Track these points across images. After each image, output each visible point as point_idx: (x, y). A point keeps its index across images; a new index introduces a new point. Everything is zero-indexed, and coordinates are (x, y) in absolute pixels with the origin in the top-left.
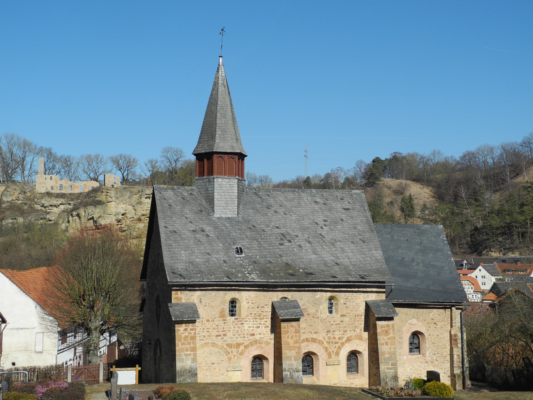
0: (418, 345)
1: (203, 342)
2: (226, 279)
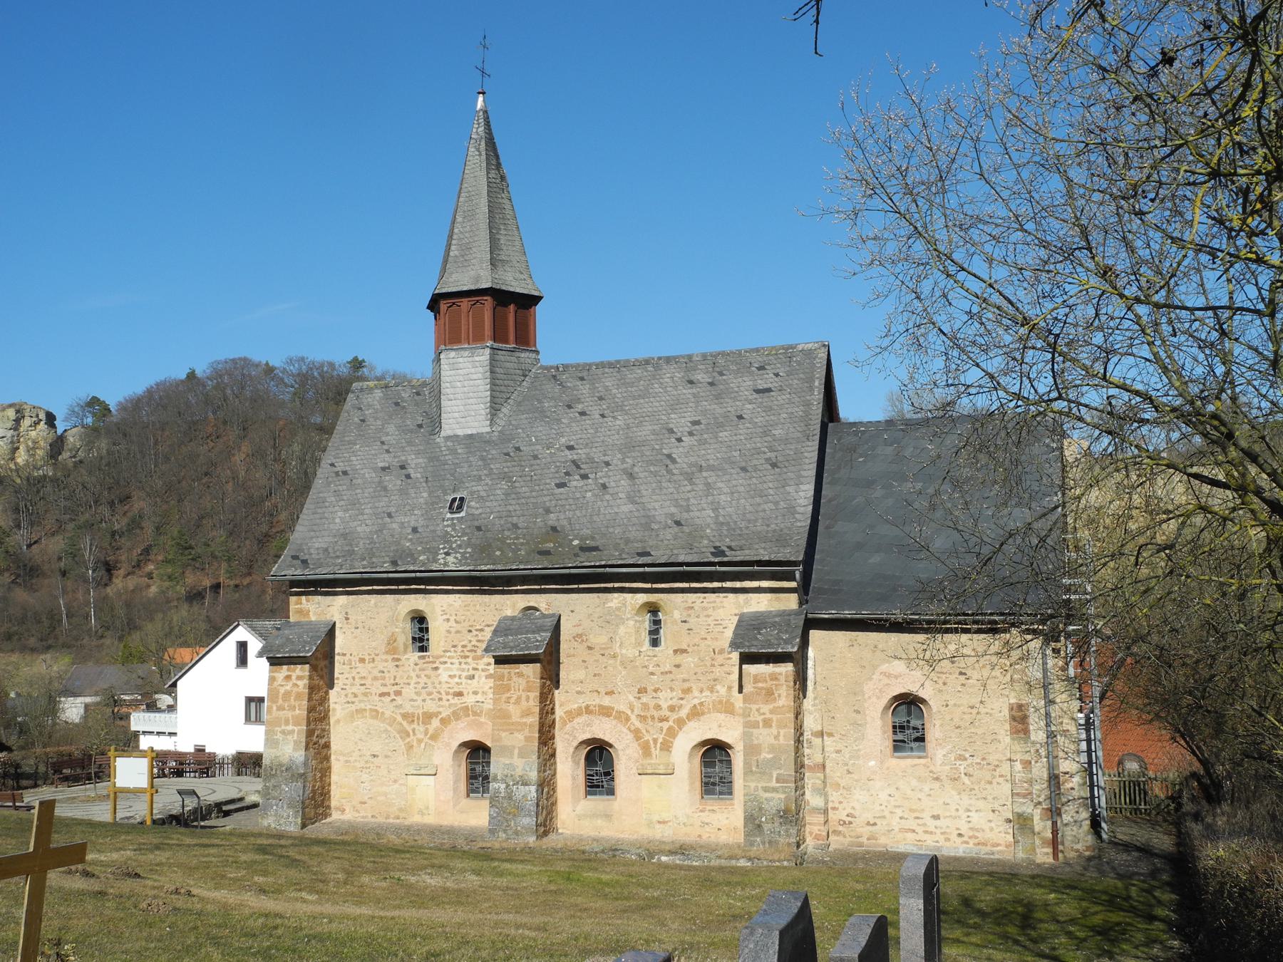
1: (353, 707)
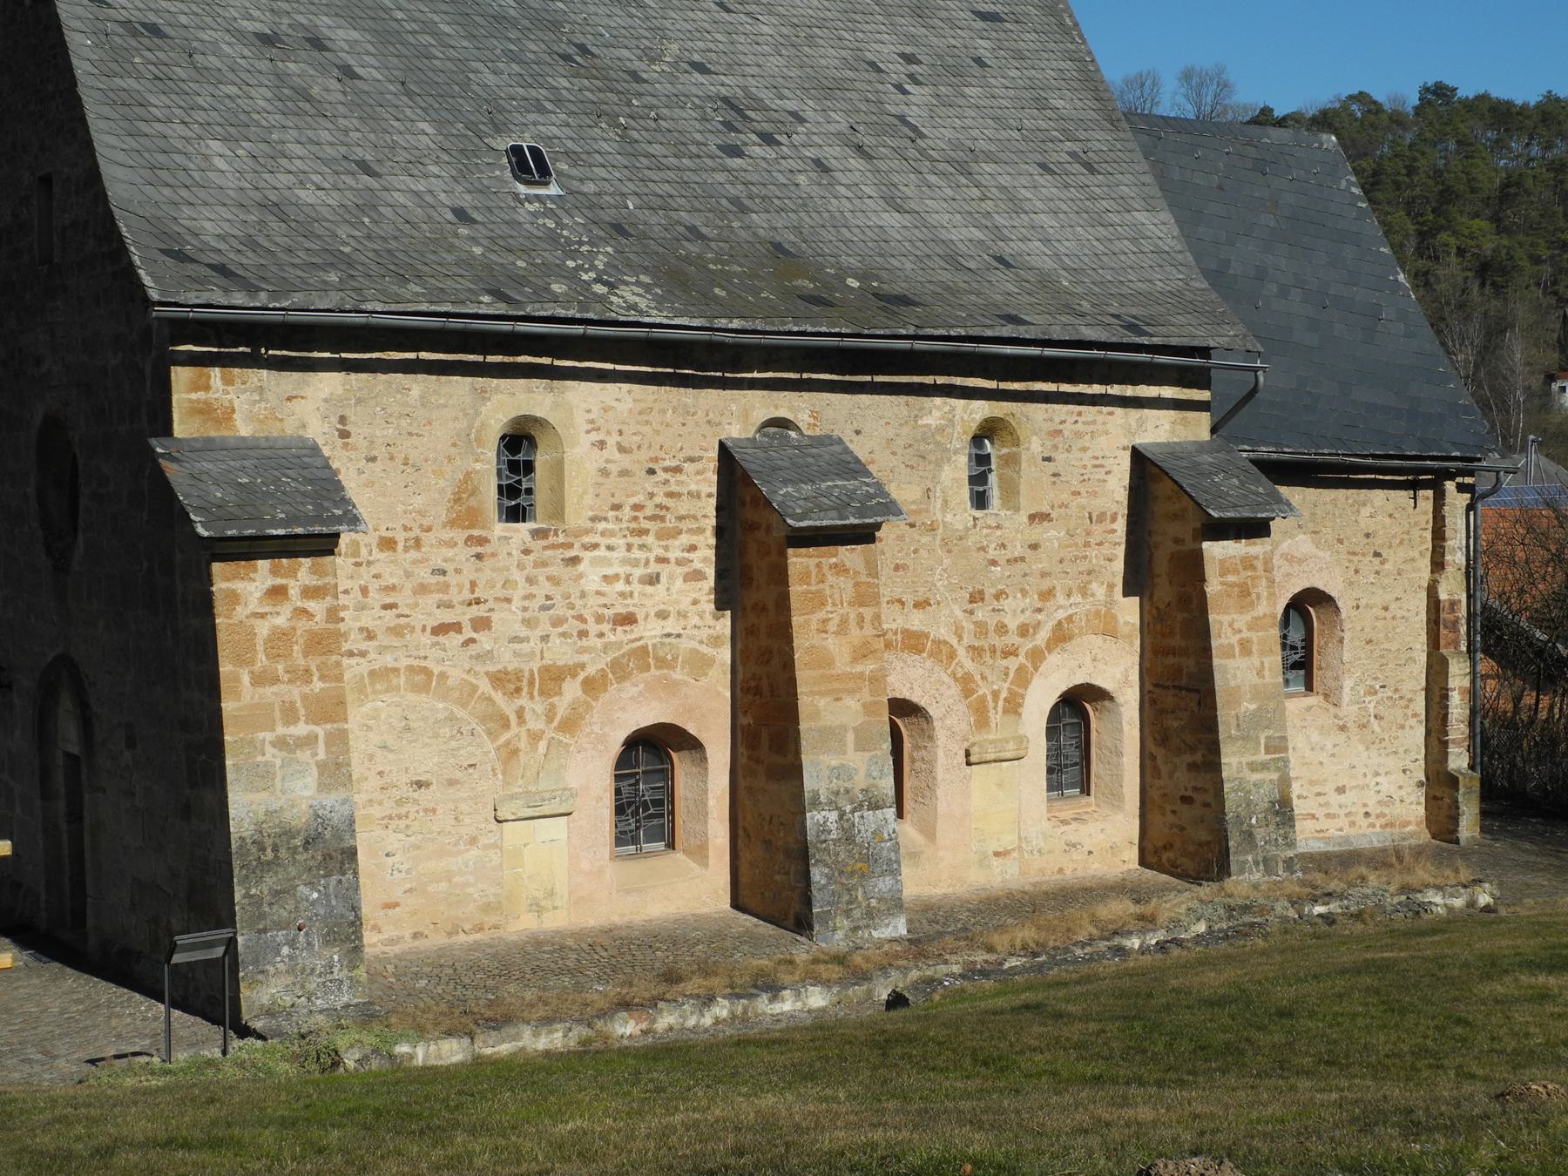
0: (1301, 653)
2: (487, 304)
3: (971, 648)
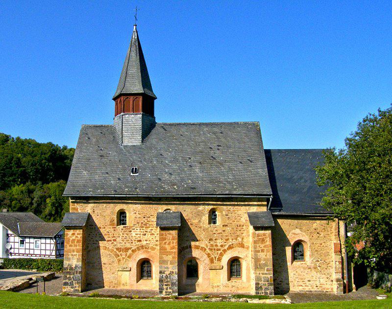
3: (209, 249)
